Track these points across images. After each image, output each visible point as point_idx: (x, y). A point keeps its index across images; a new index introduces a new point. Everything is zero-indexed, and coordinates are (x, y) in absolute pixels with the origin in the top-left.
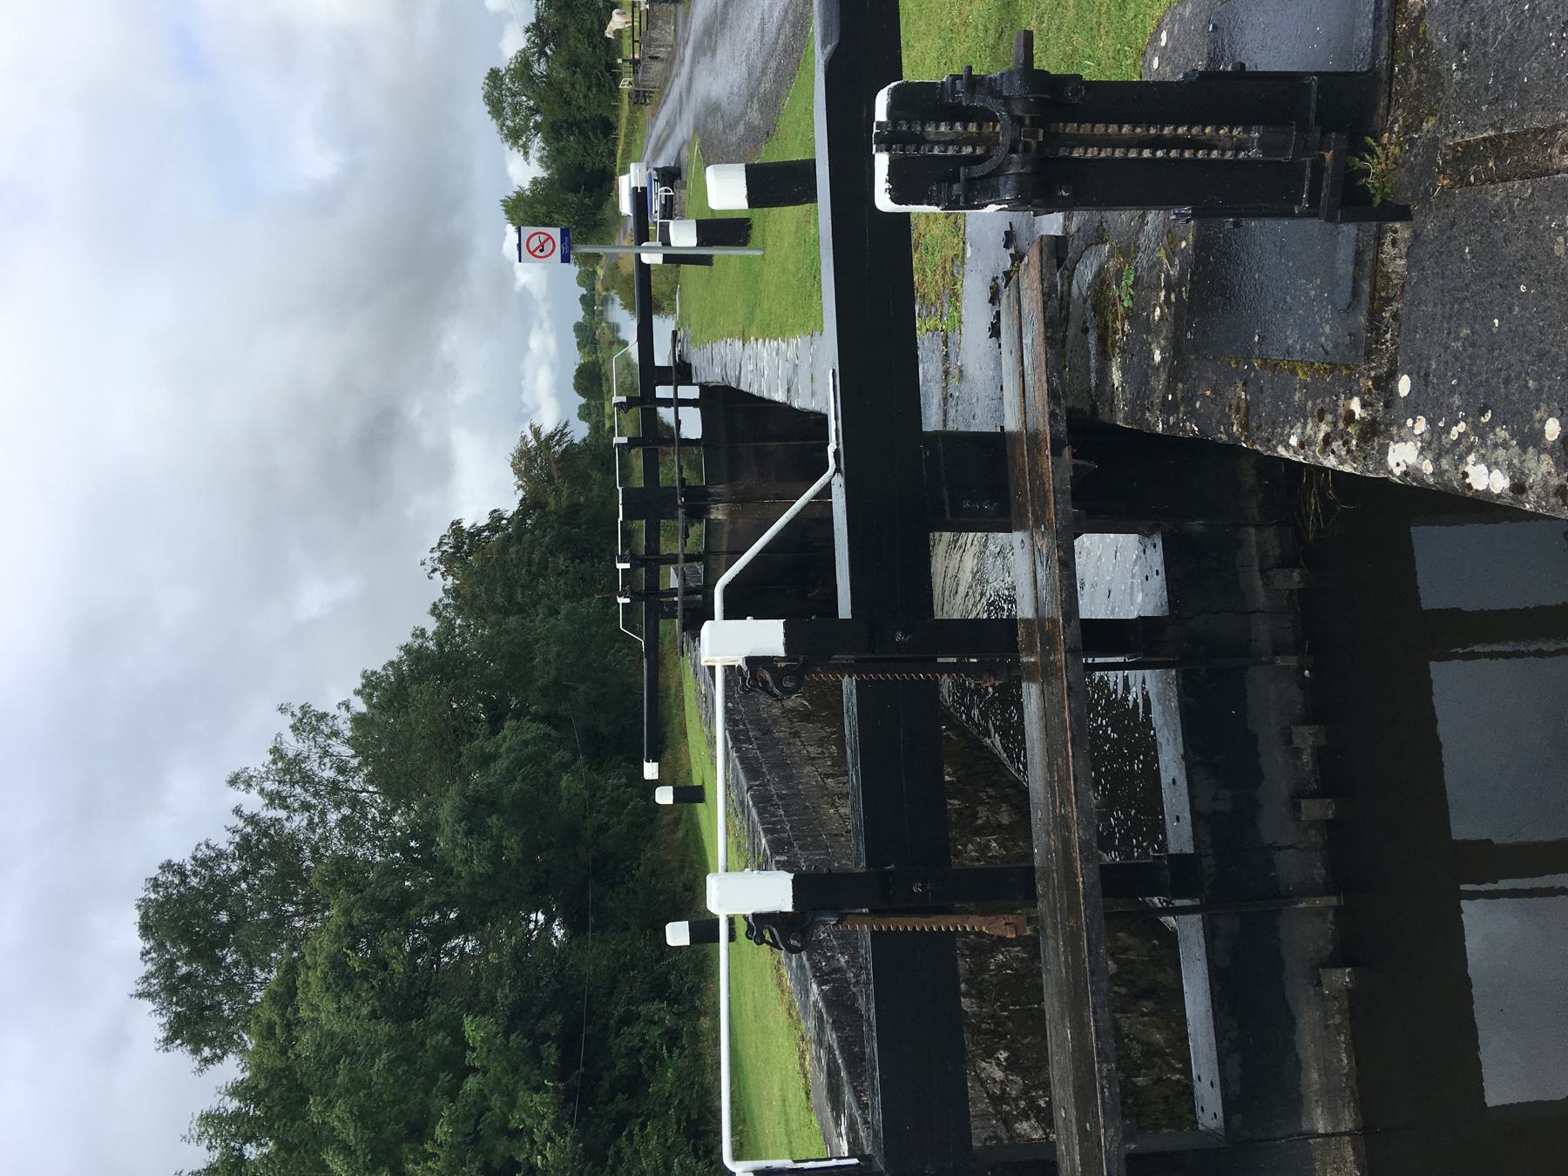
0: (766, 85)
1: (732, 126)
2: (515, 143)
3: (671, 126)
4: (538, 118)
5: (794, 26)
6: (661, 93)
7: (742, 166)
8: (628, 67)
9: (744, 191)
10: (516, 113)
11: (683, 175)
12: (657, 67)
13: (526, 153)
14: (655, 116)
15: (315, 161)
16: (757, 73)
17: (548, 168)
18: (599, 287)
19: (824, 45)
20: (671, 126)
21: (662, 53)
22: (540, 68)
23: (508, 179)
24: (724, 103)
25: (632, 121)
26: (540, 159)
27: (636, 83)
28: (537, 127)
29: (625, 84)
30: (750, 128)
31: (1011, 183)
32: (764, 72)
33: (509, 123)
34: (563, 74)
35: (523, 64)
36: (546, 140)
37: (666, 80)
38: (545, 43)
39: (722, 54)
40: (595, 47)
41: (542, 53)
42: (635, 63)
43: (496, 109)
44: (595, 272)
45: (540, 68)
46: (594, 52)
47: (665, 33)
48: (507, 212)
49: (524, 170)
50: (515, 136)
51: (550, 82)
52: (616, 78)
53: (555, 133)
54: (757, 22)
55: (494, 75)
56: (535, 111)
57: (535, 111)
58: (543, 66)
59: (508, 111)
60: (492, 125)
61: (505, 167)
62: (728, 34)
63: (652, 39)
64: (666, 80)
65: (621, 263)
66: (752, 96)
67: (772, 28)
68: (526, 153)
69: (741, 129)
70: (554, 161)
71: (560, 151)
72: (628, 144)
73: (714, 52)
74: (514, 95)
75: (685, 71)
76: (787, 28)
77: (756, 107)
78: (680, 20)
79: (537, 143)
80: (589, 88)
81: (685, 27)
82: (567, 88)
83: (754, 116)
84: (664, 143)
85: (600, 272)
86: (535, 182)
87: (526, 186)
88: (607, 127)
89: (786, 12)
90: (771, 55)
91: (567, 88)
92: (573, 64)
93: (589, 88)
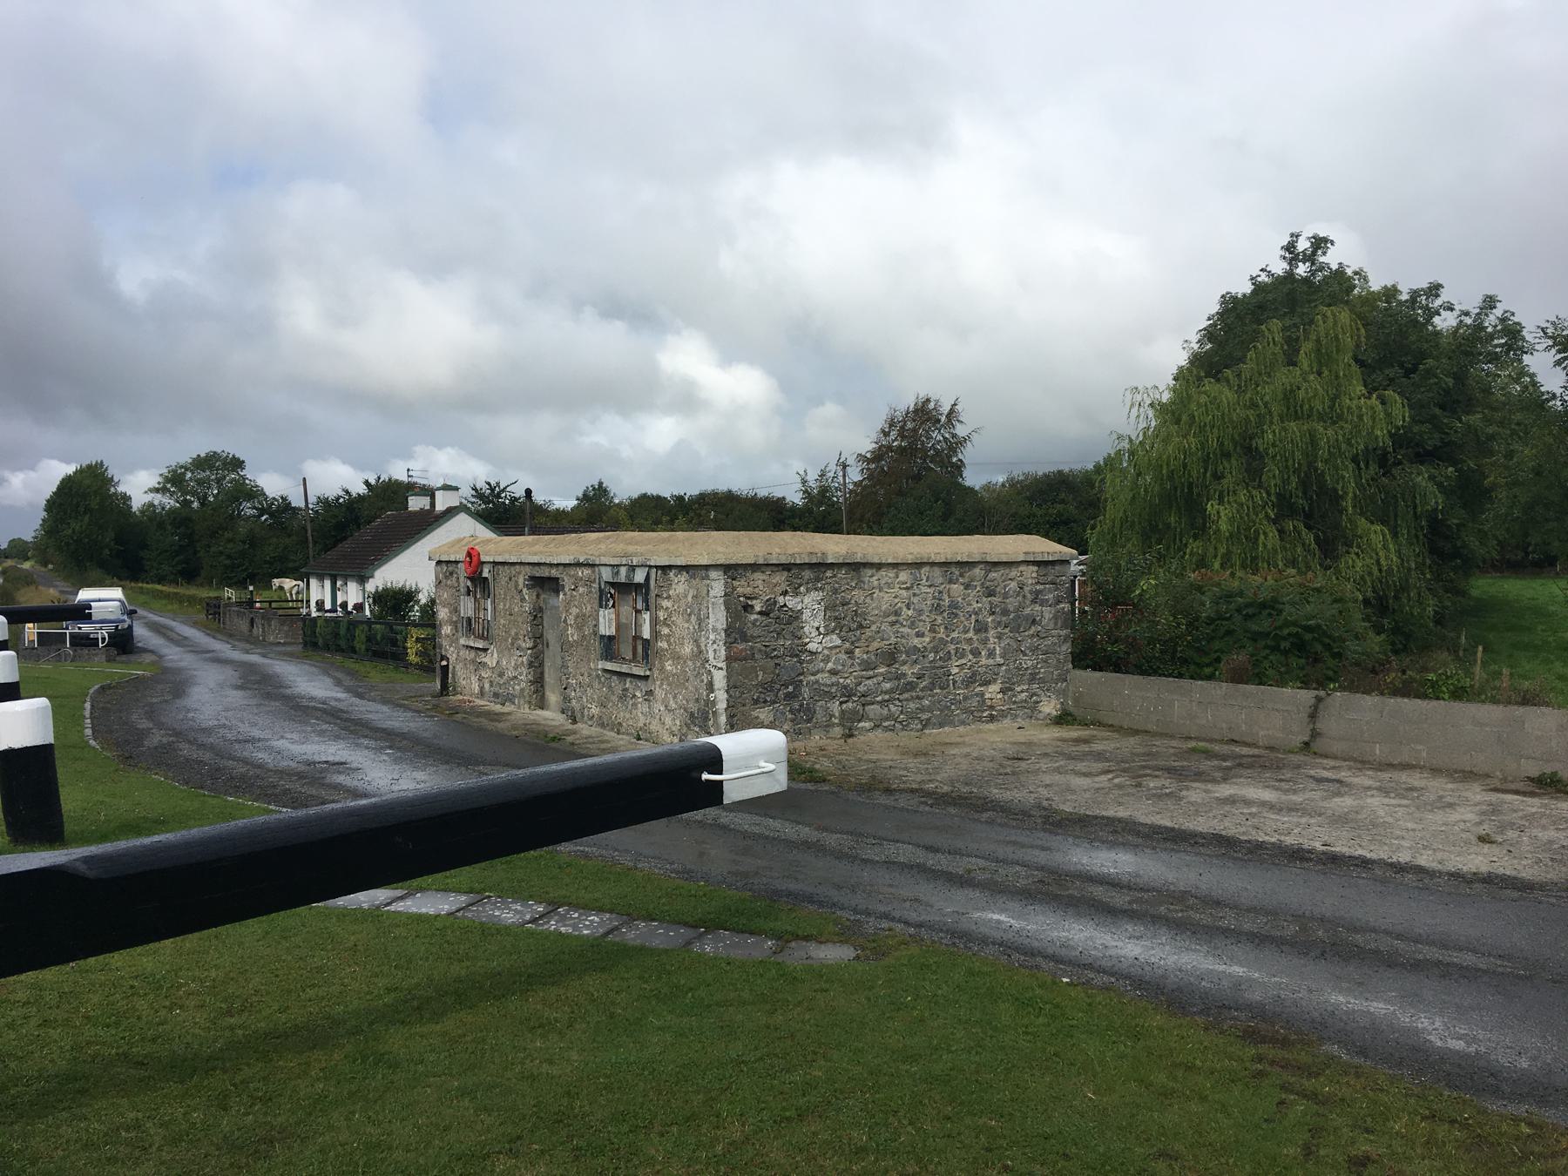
0: (186, 750)
1: (151, 714)
2: (167, 480)
3: (181, 642)
4: (195, 505)
5: (243, 777)
6: (218, 631)
7: (50, 740)
8: (245, 596)
9: (17, 745)
10: (200, 482)
11: (124, 658)
12: (244, 626)
13: (157, 490)
14: (195, 625)
15: (135, 276)
16: (203, 739)
17: (142, 512)
18: (9, 563)
19: (87, 860)
20: (181, 642)
21: (258, 631)
22: (248, 509)
23: (132, 468)
24: (180, 703)
25: (192, 600)
26: (151, 505)
27: (229, 605)
28: (186, 503)
29: (229, 593)
30: (143, 734)
31: (1363, 523)
32: (202, 746)
33: (189, 475)
34: (242, 530)
35: (254, 493)
36: (172, 511)
37: (231, 636)
38: (272, 515)
39: (236, 697)
40: (270, 563)
41: (262, 511)
42: (251, 603)
43: (202, 463)
44: (27, 559)
45: (248, 509)
46: (266, 562)
47: (276, 634)
48: (89, 467)
49: (139, 486)
50: (174, 480)
51: (234, 518)
52: (240, 584)
53: (179, 520)
54: (256, 733)
55: (237, 464)
56: (203, 501)
57: (203, 501)
58: (250, 512)
59: (202, 475)
60: (185, 458)
61: (146, 468)
62: (254, 702)
63: (269, 620)
64: (230, 636)
65: (33, 588)
66: (177, 734)
67: (248, 752)
68: (157, 490)
69: (144, 724)
70: (150, 519)
71: (161, 525)
72: (168, 596)
73: (237, 688)
74: (218, 481)
75: (237, 655)
76: (241, 769)
77: (165, 740)
78: (289, 649)
79: (169, 502)
80: (229, 557)
81: (280, 653)
82: (228, 535)
83: (157, 738)
84: (164, 635)
85: (27, 565)
86: (126, 498)
87: (121, 489)
88: (190, 574)
89: (260, 766)
90: (219, 753)
91: (228, 535)
92: (253, 541)
93: (229, 557)
